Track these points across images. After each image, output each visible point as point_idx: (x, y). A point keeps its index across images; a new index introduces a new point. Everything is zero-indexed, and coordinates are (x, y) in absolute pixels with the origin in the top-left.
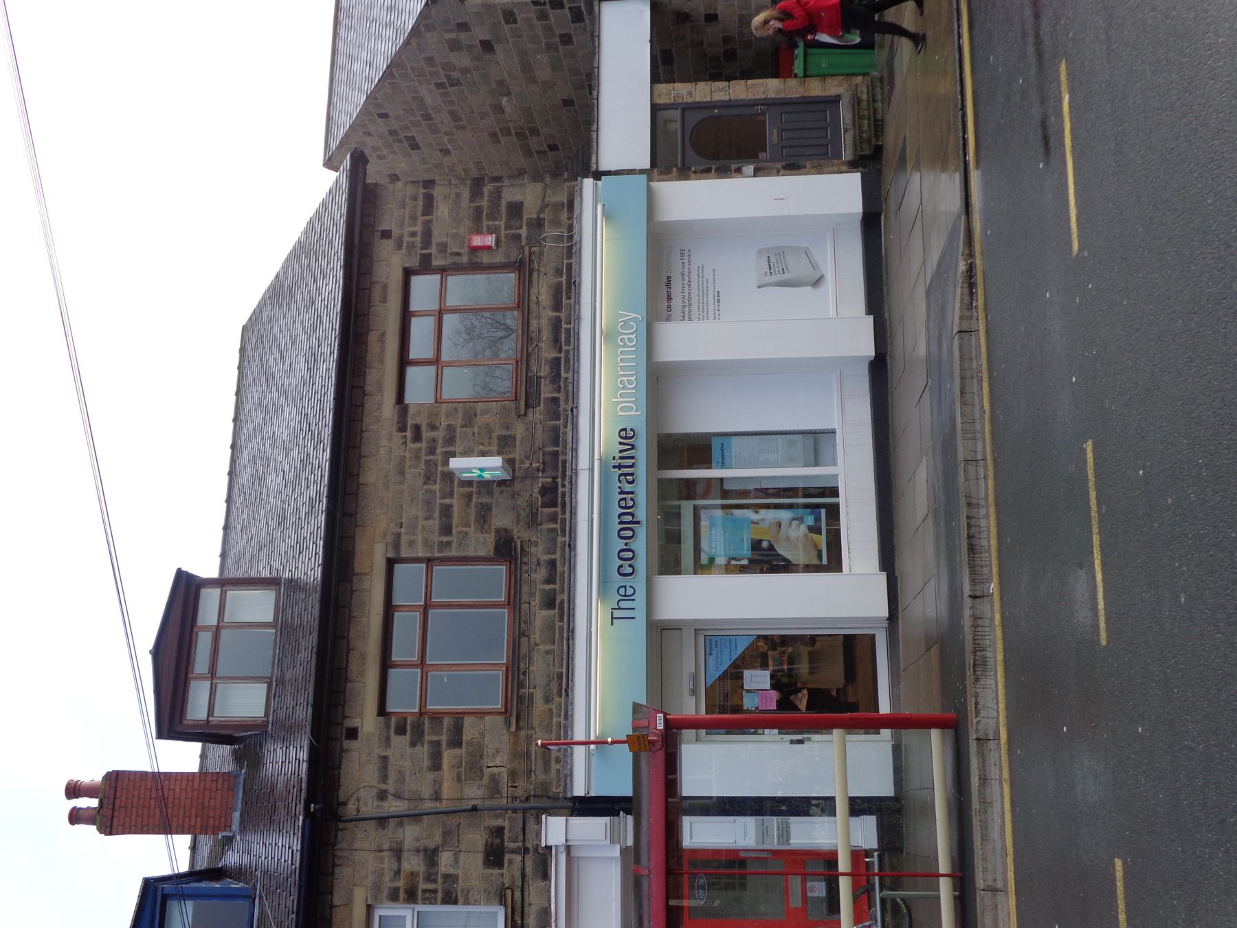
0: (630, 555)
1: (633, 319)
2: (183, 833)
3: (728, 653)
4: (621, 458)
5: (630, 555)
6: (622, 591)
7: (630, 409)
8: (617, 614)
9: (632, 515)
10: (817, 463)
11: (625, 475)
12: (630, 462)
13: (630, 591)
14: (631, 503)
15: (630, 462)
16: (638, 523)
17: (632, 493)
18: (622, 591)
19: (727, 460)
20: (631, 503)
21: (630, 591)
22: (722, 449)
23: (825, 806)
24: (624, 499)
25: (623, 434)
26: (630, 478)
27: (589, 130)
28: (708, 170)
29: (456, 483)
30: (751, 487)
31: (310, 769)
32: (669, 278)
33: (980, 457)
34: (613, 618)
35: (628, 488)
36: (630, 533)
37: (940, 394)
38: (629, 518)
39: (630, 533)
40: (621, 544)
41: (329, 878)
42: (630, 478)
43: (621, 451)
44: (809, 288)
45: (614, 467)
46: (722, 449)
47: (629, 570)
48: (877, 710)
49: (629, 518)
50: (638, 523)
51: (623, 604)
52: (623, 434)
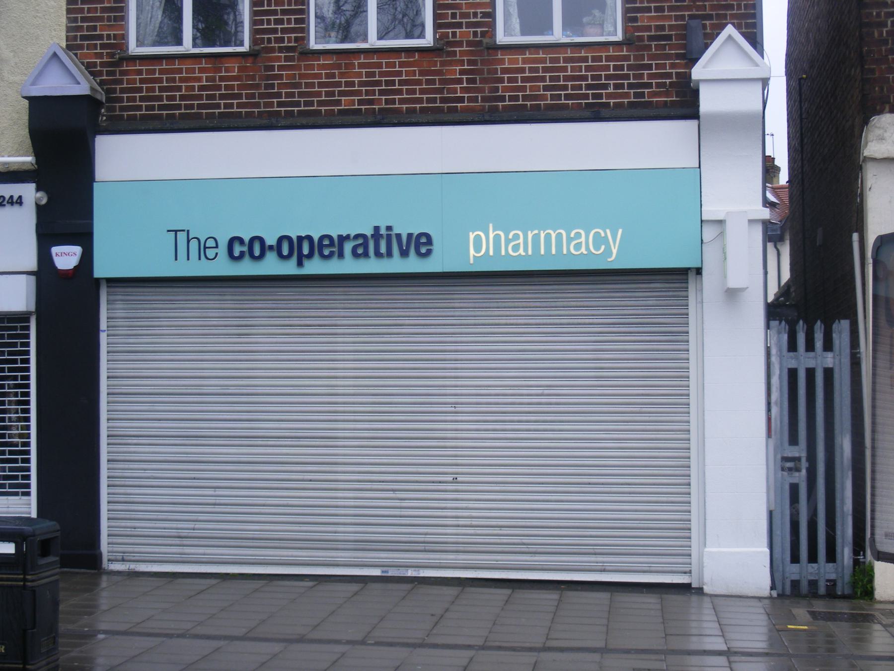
0: (257, 252)
3: (707, 639)
4: (389, 237)
5: (257, 252)
7: (478, 248)
8: (182, 237)
9: (310, 256)
11: (365, 245)
12: (383, 249)
14: (326, 252)
15: (383, 249)
17: (341, 255)
18: (211, 243)
20: (326, 252)
21: (210, 253)
26: (360, 251)
29: (257, 48)
30: (634, 656)
31: (97, 100)
34: (176, 231)
35: (348, 247)
36: (285, 252)
37: (181, 636)
38: (306, 251)
39: (285, 252)
40: (271, 241)
41: (200, 26)
42: (360, 251)
48: (21, 318)
49: (306, 251)
50: (300, 264)
51: (194, 244)
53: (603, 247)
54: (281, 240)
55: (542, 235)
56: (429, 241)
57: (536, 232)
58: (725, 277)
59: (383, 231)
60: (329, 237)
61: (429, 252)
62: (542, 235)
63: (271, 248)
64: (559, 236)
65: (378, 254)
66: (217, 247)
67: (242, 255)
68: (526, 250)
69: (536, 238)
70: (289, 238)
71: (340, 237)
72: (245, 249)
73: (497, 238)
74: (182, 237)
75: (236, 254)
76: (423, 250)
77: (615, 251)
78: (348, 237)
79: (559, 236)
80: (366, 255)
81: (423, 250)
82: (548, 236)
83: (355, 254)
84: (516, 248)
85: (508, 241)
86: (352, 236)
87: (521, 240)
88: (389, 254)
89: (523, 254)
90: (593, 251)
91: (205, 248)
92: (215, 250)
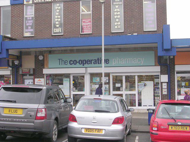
0: (75, 63)
2: (157, 27)
5: (75, 63)
8: (61, 60)
9: (85, 64)
10: (17, 83)
11: (96, 61)
12: (99, 63)
13: (66, 63)
14: (88, 63)
17: (91, 64)
18: (66, 61)
19: (33, 70)
26: (95, 63)
27: (119, 118)
28: (32, 135)
34: (60, 59)
35: (93, 62)
38: (84, 63)
45: (98, 58)
47: (71, 63)
49: (84, 63)
50: (83, 65)
51: (63, 62)
56: (108, 61)
61: (108, 63)
65: (98, 63)
74: (61, 60)
76: (107, 62)
80: (96, 63)
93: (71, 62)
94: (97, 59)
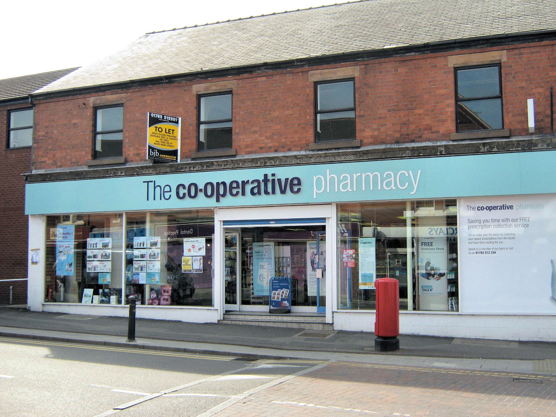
0: (193, 194)
1: (411, 186)
4: (273, 181)
5: (193, 194)
6: (167, 189)
7: (319, 187)
8: (151, 185)
9: (224, 195)
11: (259, 186)
12: (270, 190)
14: (234, 192)
15: (270, 190)
16: (218, 200)
17: (243, 194)
18: (167, 189)
20: (234, 192)
21: (167, 195)
22: (369, 243)
23: (487, 243)
24: (238, 187)
25: (296, 182)
26: (256, 191)
32: (511, 207)
33: (139, 341)
34: (148, 182)
35: (248, 188)
36: (209, 193)
38: (221, 192)
39: (209, 193)
42: (256, 191)
43: (279, 180)
44: (551, 295)
46: (369, 243)
49: (221, 192)
50: (218, 200)
51: (158, 189)
52: (296, 182)
53: (407, 184)
54: (207, 184)
55: (364, 176)
56: (299, 183)
57: (359, 174)
58: (111, 317)
59: (270, 178)
60: (237, 182)
61: (299, 190)
62: (364, 176)
63: (201, 190)
64: (375, 177)
65: (266, 193)
66: (170, 191)
67: (238, 193)
68: (352, 187)
69: (359, 179)
70: (211, 184)
71: (243, 182)
72: (186, 191)
73: (332, 179)
74: (151, 185)
75: (181, 195)
76: (295, 189)
77: (415, 187)
78: (248, 182)
79: (375, 177)
80: (259, 193)
81: (295, 189)
82: (367, 177)
83: (253, 193)
84: (345, 186)
85: (339, 182)
86: (250, 181)
87: (349, 181)
88: (274, 192)
89: (350, 190)
90: (401, 188)
91: (164, 192)
92: (169, 193)
93: (182, 191)
94: (261, 178)
